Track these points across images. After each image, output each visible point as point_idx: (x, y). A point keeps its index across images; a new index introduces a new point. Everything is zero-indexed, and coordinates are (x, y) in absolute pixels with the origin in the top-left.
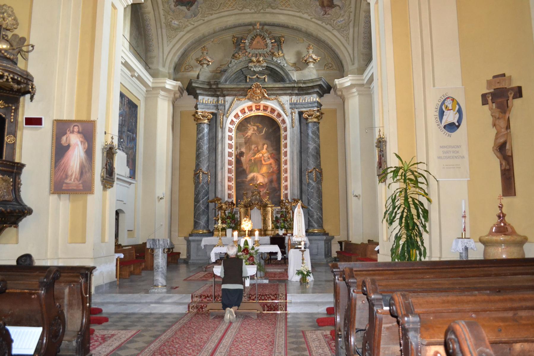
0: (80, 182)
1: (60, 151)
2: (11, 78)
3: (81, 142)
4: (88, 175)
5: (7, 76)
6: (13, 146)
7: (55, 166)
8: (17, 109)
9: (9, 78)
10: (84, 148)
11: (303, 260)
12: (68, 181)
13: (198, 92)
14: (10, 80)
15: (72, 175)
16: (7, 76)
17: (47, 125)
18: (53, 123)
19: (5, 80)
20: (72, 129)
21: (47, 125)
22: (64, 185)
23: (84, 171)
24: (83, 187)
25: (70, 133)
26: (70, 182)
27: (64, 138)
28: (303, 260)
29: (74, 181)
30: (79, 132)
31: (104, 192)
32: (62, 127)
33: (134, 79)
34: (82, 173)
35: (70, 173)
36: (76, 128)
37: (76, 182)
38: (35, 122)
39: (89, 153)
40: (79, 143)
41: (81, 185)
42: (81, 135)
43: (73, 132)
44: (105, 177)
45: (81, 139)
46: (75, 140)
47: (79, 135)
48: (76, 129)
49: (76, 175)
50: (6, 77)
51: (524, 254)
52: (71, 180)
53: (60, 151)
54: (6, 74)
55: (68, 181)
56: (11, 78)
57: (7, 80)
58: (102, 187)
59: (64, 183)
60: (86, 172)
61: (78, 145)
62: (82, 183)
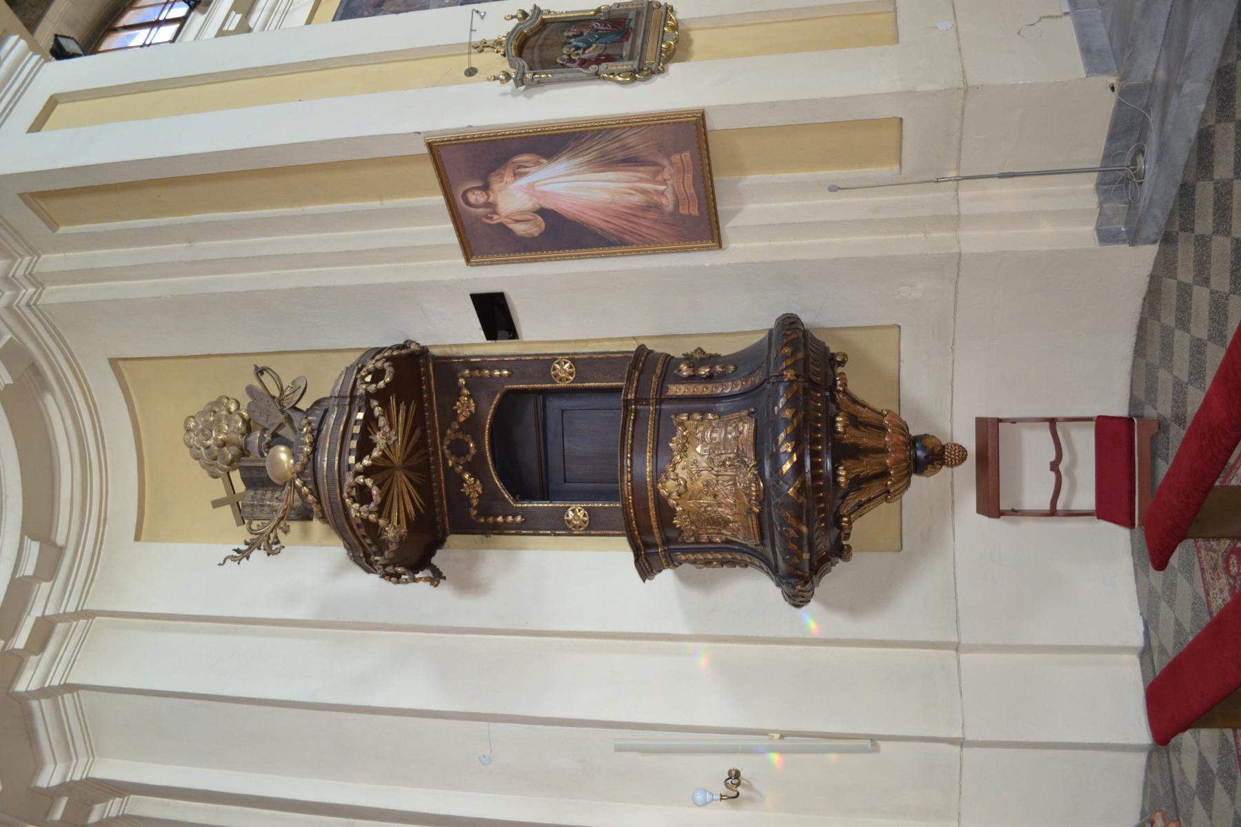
0: (665, 162)
1: (562, 234)
2: (359, 459)
3: (517, 175)
4: (632, 139)
5: (357, 474)
6: (558, 526)
7: (622, 243)
8: (467, 362)
9: (359, 466)
10: (538, 163)
11: (960, 49)
12: (668, 203)
13: (61, 611)
14: (366, 462)
15: (644, 192)
16: (357, 474)
17: (492, 277)
18: (478, 264)
19: (369, 482)
20: (481, 211)
21: (492, 277)
22: (683, 211)
23: (620, 155)
24: (680, 151)
25: (495, 213)
26: (669, 195)
27: (519, 229)
28: (960, 49)
29: (664, 182)
30: (486, 188)
31: (699, 39)
32: (480, 238)
33: (256, 19)
34: (630, 161)
35: (638, 199)
36: (472, 198)
37: (666, 176)
38: (494, 313)
39: (550, 143)
40: (523, 182)
41: (676, 158)
42: (494, 179)
43: (491, 206)
44: (634, 64)
45: (508, 178)
46: (516, 196)
47: (496, 186)
48: (477, 197)
49: (641, 180)
50: (360, 479)
51: (1135, 648)
52: (662, 193)
53: (562, 234)
54: (349, 479)
55: (668, 203)
56: (359, 459)
57: (367, 472)
58: (673, 68)
59: (675, 213)
60: (624, 148)
61: (532, 185)
62: (668, 156)
